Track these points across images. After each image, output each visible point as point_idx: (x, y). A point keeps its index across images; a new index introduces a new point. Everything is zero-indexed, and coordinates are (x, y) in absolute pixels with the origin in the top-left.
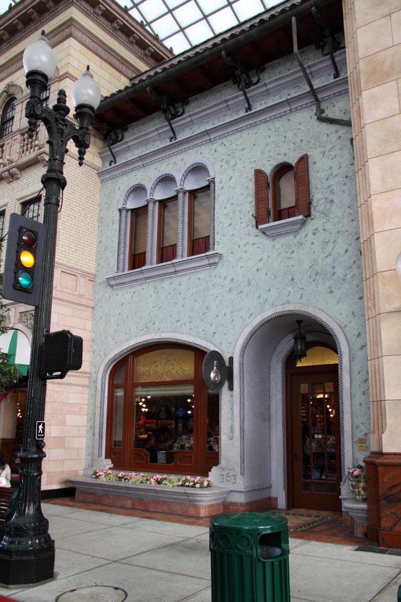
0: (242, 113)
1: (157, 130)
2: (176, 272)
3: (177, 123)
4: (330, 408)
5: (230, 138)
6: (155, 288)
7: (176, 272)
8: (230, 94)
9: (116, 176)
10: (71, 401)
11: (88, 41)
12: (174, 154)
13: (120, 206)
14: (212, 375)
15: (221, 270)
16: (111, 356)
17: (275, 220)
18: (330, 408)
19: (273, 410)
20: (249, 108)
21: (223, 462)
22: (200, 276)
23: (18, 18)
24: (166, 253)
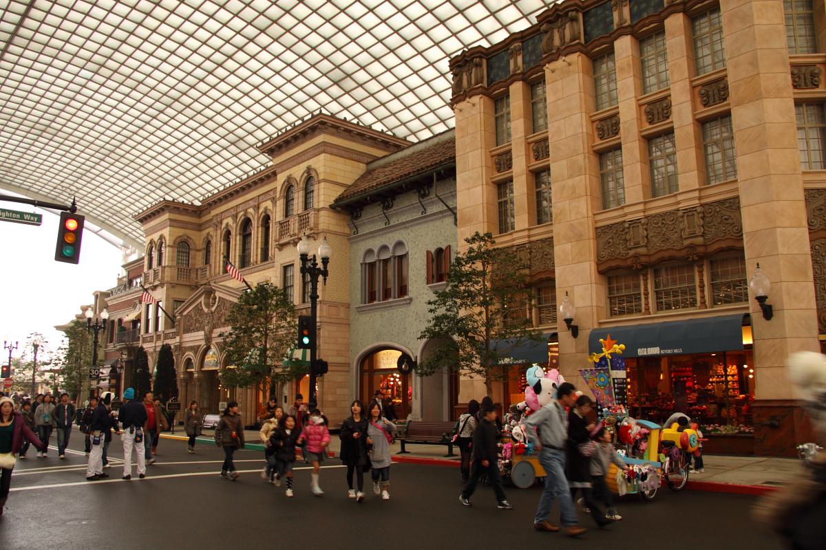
0: (419, 215)
1: (378, 215)
2: (391, 306)
3: (390, 212)
4: (629, 390)
5: (416, 227)
6: (381, 315)
7: (391, 306)
8: (413, 199)
9: (358, 241)
10: (339, 381)
11: (335, 151)
12: (388, 233)
13: (362, 262)
14: (403, 367)
15: (412, 307)
16: (360, 354)
17: (438, 282)
18: (629, 390)
19: (444, 384)
20: (425, 211)
21: (413, 412)
22: (403, 310)
23: (292, 137)
24: (387, 295)
